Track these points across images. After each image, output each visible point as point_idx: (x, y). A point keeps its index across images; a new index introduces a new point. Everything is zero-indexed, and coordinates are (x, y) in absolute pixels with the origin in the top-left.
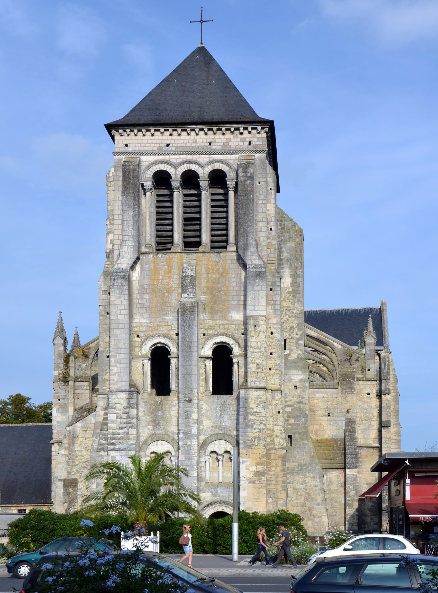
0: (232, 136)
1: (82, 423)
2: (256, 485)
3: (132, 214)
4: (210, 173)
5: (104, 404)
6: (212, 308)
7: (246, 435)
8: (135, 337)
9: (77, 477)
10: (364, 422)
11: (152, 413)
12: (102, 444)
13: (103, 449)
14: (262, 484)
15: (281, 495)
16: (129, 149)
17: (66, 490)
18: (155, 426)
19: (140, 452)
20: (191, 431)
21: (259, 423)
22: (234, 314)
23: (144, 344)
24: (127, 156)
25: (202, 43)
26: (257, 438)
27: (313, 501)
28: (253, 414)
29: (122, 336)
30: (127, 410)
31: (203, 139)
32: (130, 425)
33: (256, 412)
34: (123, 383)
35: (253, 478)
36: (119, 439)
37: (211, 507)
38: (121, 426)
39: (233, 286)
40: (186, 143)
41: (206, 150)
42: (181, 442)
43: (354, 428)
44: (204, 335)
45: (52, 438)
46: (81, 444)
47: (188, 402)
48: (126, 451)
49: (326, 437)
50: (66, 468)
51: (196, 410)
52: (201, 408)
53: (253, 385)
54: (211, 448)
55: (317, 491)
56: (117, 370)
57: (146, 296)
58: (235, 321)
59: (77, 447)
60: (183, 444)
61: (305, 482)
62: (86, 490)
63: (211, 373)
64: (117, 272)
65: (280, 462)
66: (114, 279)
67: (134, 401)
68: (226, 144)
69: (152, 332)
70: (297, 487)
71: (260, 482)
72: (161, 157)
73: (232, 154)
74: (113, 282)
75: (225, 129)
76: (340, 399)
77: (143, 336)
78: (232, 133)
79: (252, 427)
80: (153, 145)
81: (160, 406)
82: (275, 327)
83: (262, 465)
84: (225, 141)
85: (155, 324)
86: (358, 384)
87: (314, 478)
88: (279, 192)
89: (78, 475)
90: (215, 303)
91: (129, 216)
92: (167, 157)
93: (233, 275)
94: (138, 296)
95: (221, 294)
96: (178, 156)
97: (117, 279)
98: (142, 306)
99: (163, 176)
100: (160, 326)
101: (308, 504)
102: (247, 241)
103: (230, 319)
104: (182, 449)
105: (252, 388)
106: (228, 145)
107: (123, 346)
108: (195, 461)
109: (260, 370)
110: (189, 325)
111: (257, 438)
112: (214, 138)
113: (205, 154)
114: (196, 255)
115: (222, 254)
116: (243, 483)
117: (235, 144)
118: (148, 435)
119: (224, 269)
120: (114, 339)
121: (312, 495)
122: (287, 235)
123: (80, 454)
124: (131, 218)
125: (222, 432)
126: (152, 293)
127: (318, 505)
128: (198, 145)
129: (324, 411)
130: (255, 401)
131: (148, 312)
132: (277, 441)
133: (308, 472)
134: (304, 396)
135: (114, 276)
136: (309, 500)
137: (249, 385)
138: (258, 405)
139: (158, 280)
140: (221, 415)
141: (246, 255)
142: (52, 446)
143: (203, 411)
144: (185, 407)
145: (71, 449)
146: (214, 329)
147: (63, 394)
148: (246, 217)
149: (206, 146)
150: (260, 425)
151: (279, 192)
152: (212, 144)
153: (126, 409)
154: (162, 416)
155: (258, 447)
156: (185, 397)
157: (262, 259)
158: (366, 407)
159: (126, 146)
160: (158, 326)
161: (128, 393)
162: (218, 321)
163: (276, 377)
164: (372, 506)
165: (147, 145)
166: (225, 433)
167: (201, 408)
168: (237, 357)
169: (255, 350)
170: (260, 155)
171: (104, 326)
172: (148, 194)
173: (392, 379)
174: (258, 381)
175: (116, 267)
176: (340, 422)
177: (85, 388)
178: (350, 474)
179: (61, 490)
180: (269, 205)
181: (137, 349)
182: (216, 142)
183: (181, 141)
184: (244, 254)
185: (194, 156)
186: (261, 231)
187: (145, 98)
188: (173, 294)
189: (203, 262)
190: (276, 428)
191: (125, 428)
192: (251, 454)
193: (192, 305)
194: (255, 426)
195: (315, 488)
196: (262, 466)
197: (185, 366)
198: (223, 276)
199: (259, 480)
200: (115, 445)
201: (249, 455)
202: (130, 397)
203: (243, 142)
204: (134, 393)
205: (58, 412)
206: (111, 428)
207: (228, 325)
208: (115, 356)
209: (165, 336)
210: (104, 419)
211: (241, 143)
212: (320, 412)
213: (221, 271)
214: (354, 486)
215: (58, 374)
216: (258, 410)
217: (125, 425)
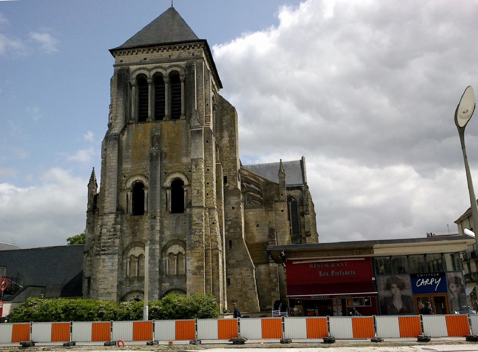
0: (183, 51)
11: (131, 227)
29: (113, 177)
38: (110, 237)
44: (166, 173)
49: (257, 241)
51: (158, 224)
54: (170, 250)
61: (241, 273)
67: (119, 219)
70: (236, 277)
72: (141, 66)
76: (264, 215)
78: (183, 49)
87: (247, 270)
88: (221, 87)
90: (173, 152)
101: (244, 290)
105: (194, 207)
107: (113, 183)
122: (225, 112)
137: (193, 205)
138: (199, 218)
140: (176, 227)
144: (152, 222)
151: (221, 87)
156: (152, 215)
159: (121, 61)
168: (186, 186)
172: (133, 88)
173: (310, 205)
175: (112, 133)
181: (124, 185)
189: (167, 126)
194: (196, 233)
202: (117, 216)
206: (103, 239)
208: (108, 190)
209: (142, 175)
213: (176, 132)
216: (198, 222)
217: (112, 237)
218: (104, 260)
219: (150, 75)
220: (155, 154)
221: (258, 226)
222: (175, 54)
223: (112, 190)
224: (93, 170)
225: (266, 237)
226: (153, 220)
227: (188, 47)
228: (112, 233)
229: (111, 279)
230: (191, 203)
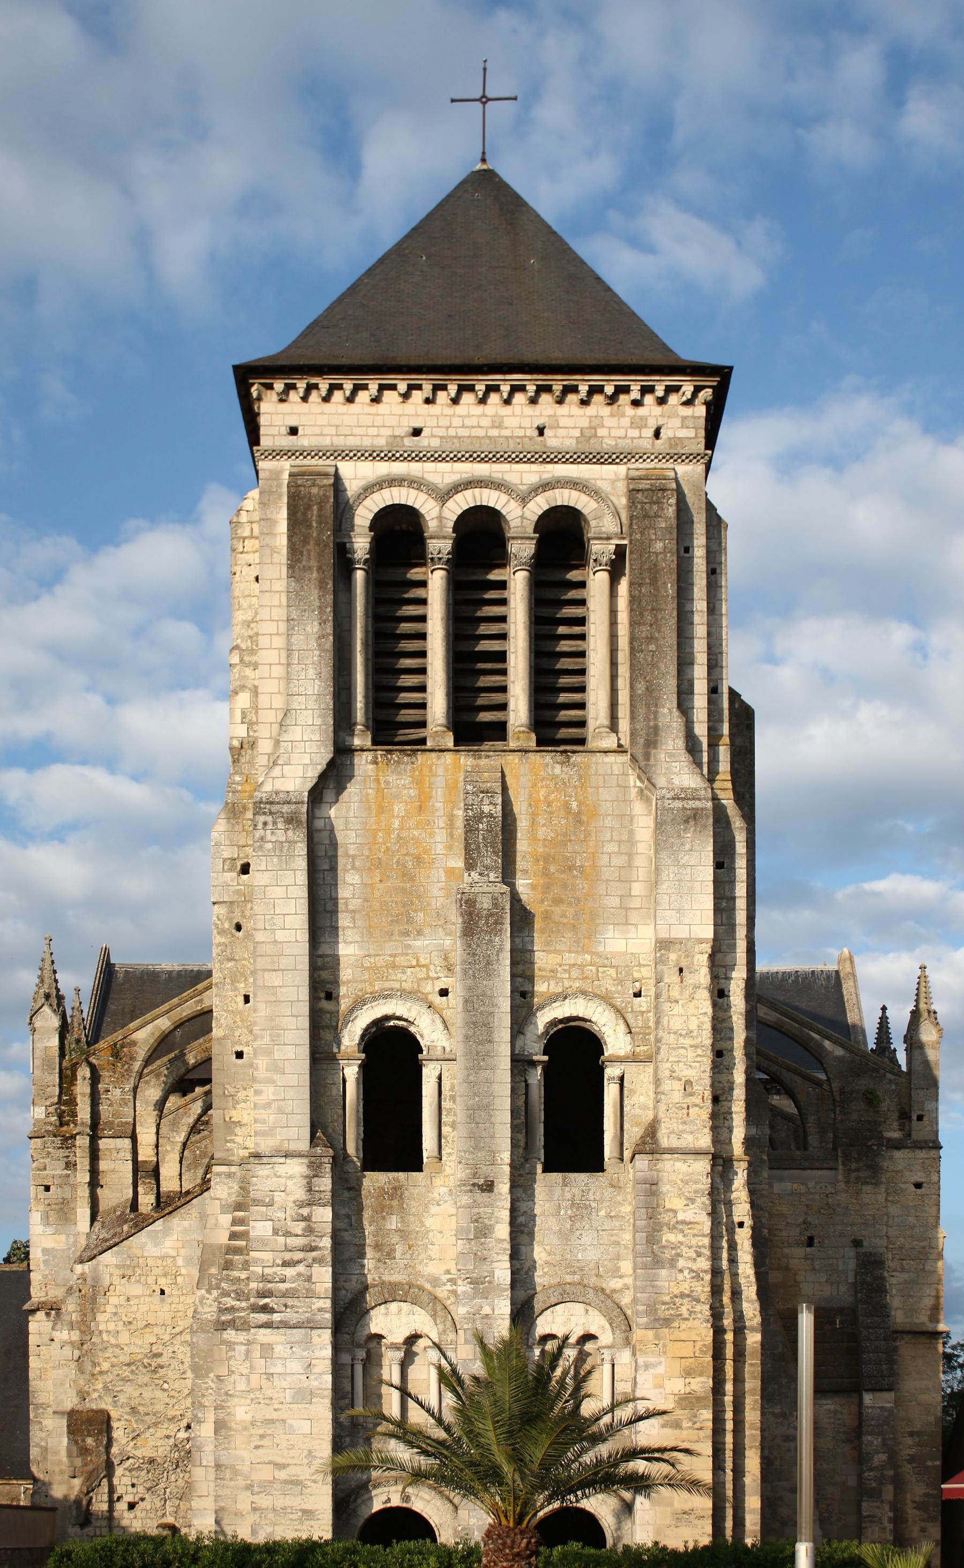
0: (606, 411)
1: (117, 1253)
2: (685, 1432)
3: (315, 630)
4: (541, 517)
5: (229, 1194)
7: (656, 1287)
9: (106, 1404)
12: (232, 1309)
13: (232, 1324)
14: (701, 1429)
16: (302, 441)
17: (76, 1442)
18: (379, 1260)
21: (694, 1255)
22: (610, 935)
24: (298, 462)
25: (483, 160)
26: (688, 1296)
27: (779, 1480)
28: (674, 1228)
30: (305, 1211)
31: (522, 416)
32: (314, 1254)
33: (684, 1222)
36: (284, 1295)
38: (288, 1256)
39: (610, 854)
40: (473, 427)
41: (532, 449)
43: (883, 1278)
45: (29, 1297)
46: (115, 1314)
47: (483, 1191)
48: (303, 1331)
50: (75, 1381)
53: (674, 1143)
56: (274, 1094)
58: (614, 954)
59: (104, 1321)
60: (468, 1313)
62: (132, 1444)
64: (272, 803)
66: (265, 824)
68: (588, 434)
71: (694, 1423)
72: (398, 468)
74: (259, 833)
75: (587, 388)
80: (373, 431)
84: (586, 424)
85: (380, 962)
86: (891, 1158)
89: (109, 1399)
90: (558, 901)
91: (307, 636)
92: (414, 468)
93: (609, 822)
96: (449, 465)
99: (397, 528)
100: (394, 966)
102: (656, 718)
103: (601, 948)
105: (672, 1151)
106: (596, 436)
107: (290, 1022)
110: (488, 963)
111: (688, 1296)
112: (555, 416)
113: (529, 461)
115: (575, 758)
117: (614, 433)
120: (266, 1002)
121: (777, 1463)
123: (113, 1341)
125: (577, 1278)
126: (370, 869)
128: (507, 433)
129: (798, 1230)
135: (264, 813)
137: (665, 1141)
141: (652, 759)
142: (30, 1318)
144: (475, 1205)
145: (85, 1325)
146: (555, 977)
147: (59, 1172)
148: (652, 647)
149: (531, 438)
152: (546, 431)
156: (475, 1175)
158: (912, 1220)
159: (294, 431)
161: (305, 1160)
164: (926, 1495)
165: (357, 431)
166: (585, 1281)
169: (682, 1040)
171: (230, 964)
174: (692, 1133)
176: (840, 1262)
177: (121, 1154)
178: (873, 1407)
179: (60, 1442)
182: (558, 427)
183: (457, 422)
185: (496, 467)
187: (340, 300)
189: (530, 774)
191: (299, 1262)
192: (670, 1344)
193: (496, 905)
194: (681, 1263)
197: (476, 1083)
198: (580, 822)
200: (272, 1311)
201: (664, 1346)
203: (640, 428)
204: (326, 1160)
205: (46, 1220)
206: (256, 1261)
207: (594, 969)
209: (606, 999)
210: (233, 1236)
211: (634, 433)
214: (884, 1440)
215: (43, 1116)
217: (299, 1255)
219: (439, 520)
220: (485, 903)
221: (810, 1242)
222: (569, 420)
223: (290, 1052)
225: (843, 1288)
226: (482, 1197)
227: (635, 394)
228: (301, 1241)
230: (652, 1131)
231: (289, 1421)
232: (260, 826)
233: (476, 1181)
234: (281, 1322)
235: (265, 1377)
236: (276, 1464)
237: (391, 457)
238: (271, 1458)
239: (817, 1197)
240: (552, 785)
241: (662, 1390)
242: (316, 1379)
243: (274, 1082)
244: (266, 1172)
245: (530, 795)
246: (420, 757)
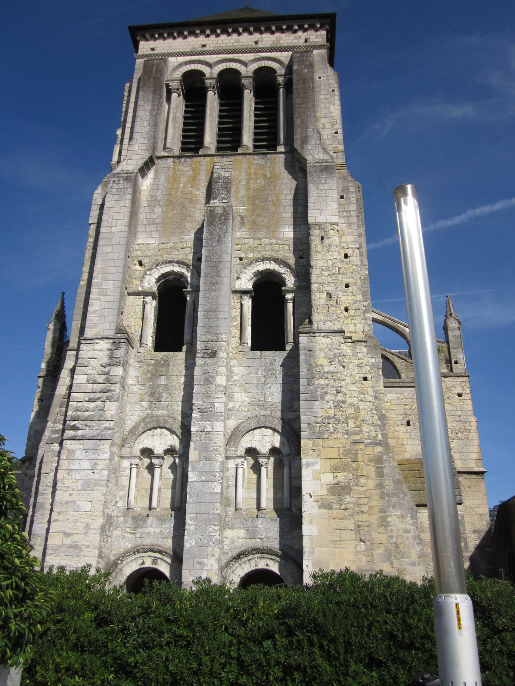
2: (335, 512)
6: (254, 223)
8: (135, 264)
10: (459, 435)
11: (150, 380)
14: (346, 509)
15: (379, 535)
18: (152, 402)
19: (123, 448)
20: (213, 406)
21: (335, 392)
22: (286, 230)
23: (148, 273)
27: (404, 558)
29: (116, 256)
30: (107, 370)
32: (107, 394)
33: (328, 373)
34: (107, 326)
35: (327, 497)
37: (244, 560)
38: (92, 395)
42: (195, 426)
44: (241, 259)
47: (210, 357)
49: (407, 456)
51: (223, 370)
52: (232, 372)
53: (322, 327)
55: (410, 540)
57: (158, 209)
63: (250, 317)
65: (372, 470)
66: (114, 181)
67: (120, 353)
69: (162, 257)
71: (341, 505)
73: (283, 51)
77: (147, 263)
79: (323, 399)
81: (164, 369)
82: (350, 246)
83: (344, 470)
87: (403, 516)
90: (259, 216)
92: (202, 58)
94: (147, 210)
95: (268, 205)
97: (119, 181)
98: (151, 222)
102: (306, 133)
103: (282, 236)
104: (195, 439)
108: (218, 463)
109: (333, 303)
110: (219, 238)
111: (333, 418)
114: (232, 158)
116: (309, 507)
118: (139, 418)
119: (271, 174)
120: (102, 260)
121: (401, 546)
124: (148, 113)
125: (268, 412)
127: (413, 564)
130: (325, 353)
131: (159, 229)
132: (366, 429)
133: (394, 508)
134: (378, 388)
136: (398, 557)
139: (177, 189)
143: (236, 377)
148: (304, 106)
150: (336, 395)
153: (104, 367)
154: (165, 385)
155: (335, 435)
156: (206, 348)
157: (328, 153)
158: (459, 413)
160: (171, 248)
161: (111, 341)
162: (263, 240)
163: (357, 320)
167: (232, 372)
170: (320, 51)
172: (174, 95)
180: (332, 107)
184: (302, 148)
186: (324, 128)
188: (198, 205)
190: (362, 406)
193: (224, 211)
194: (327, 398)
195: (406, 535)
196: (345, 474)
197: (209, 298)
198: (271, 182)
199: (340, 502)
212: (395, 419)
213: (268, 175)
216: (332, 368)
217: (100, 395)
218: (71, 452)
222: (267, 39)
223: (111, 284)
224: (63, 299)
226: (209, 360)
228: (101, 387)
229: (87, 506)
231: (78, 503)
232: (111, 182)
233: (206, 351)
234: (82, 436)
235: (66, 472)
236: (65, 533)
237: (191, 54)
238: (62, 529)
239: (409, 400)
240: (258, 167)
241: (319, 481)
242: (98, 473)
243: (100, 300)
244: (88, 348)
245: (247, 171)
246: (195, 160)
